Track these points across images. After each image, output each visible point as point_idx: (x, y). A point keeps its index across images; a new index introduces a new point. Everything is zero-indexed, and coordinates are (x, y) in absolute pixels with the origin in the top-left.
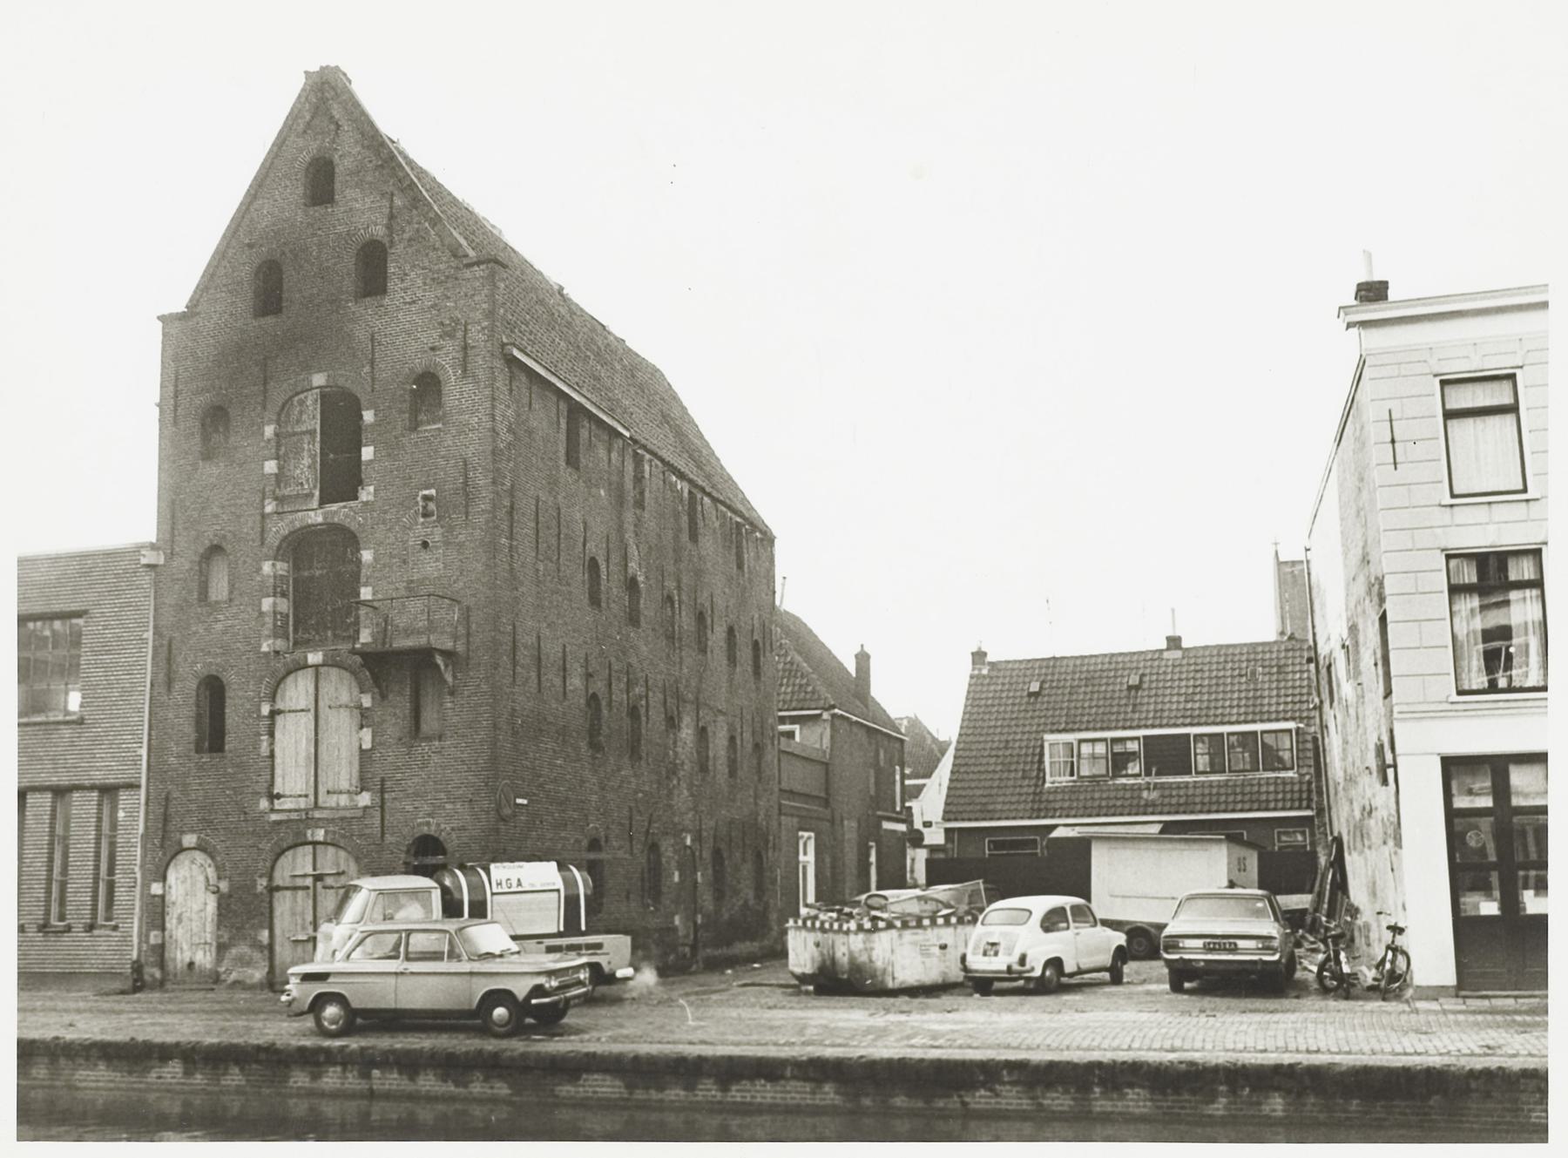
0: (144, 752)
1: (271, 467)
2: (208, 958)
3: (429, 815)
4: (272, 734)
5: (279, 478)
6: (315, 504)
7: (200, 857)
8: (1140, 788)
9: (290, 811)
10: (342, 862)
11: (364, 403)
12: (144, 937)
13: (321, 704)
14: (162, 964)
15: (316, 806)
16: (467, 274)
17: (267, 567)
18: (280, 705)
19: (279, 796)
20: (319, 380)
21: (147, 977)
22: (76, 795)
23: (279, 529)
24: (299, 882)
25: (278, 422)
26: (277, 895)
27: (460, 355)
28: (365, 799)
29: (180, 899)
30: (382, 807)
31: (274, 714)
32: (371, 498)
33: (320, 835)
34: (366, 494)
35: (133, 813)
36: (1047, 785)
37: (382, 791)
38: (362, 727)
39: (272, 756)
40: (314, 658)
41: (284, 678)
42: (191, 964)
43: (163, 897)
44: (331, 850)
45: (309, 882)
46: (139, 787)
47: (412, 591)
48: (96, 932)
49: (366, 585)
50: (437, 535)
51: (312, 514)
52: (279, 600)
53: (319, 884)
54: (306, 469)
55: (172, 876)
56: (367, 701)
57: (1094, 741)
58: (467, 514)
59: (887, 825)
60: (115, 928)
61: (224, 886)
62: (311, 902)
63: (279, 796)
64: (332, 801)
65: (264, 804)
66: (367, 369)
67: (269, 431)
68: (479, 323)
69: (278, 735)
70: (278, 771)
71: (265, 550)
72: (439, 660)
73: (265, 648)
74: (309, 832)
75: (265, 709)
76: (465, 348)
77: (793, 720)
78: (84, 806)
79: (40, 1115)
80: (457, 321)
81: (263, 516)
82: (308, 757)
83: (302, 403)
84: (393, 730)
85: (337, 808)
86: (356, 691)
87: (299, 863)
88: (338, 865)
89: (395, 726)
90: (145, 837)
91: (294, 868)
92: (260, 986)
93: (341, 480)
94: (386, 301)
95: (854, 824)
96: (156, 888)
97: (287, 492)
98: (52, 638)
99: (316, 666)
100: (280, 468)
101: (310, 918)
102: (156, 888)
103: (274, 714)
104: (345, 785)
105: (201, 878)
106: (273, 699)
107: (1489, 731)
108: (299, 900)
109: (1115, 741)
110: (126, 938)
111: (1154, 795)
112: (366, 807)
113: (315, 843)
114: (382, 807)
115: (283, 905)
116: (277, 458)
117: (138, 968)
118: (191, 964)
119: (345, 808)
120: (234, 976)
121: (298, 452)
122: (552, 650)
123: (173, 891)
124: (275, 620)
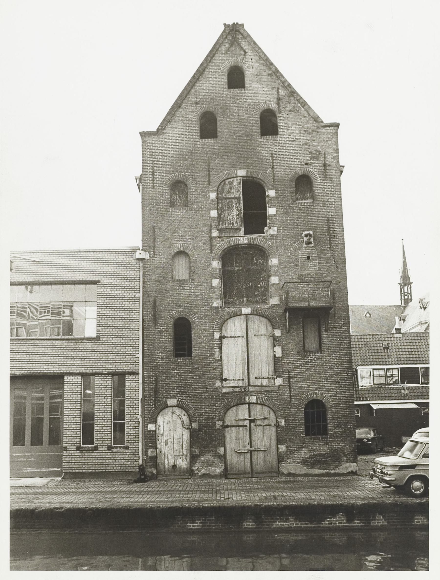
0: (140, 356)
2: (185, 462)
4: (220, 348)
7: (178, 411)
8: (399, 389)
9: (234, 387)
10: (266, 413)
12: (145, 453)
13: (249, 333)
14: (156, 466)
15: (249, 385)
16: (324, 130)
18: (224, 334)
19: (226, 380)
20: (242, 173)
21: (147, 472)
22: (97, 378)
23: (221, 245)
24: (240, 423)
26: (227, 430)
27: (323, 168)
28: (279, 381)
29: (166, 433)
30: (290, 386)
31: (222, 338)
32: (275, 233)
33: (253, 399)
35: (135, 388)
36: (360, 387)
37: (289, 378)
38: (274, 346)
39: (221, 359)
40: (246, 310)
42: (174, 466)
43: (155, 431)
44: (259, 407)
45: (247, 423)
46: (138, 374)
47: (302, 279)
49: (275, 275)
50: (314, 254)
51: (241, 238)
53: (252, 424)
54: (234, 215)
55: (160, 420)
56: (278, 333)
57: (379, 369)
58: (330, 245)
60: (127, 448)
61: (195, 425)
62: (248, 433)
63: (226, 380)
64: (258, 382)
65: (218, 384)
66: (269, 170)
67: (213, 196)
68: (332, 154)
69: (223, 348)
70: (225, 367)
71: (213, 255)
73: (215, 304)
74: (247, 398)
75: (217, 336)
76: (325, 165)
79: (21, 554)
80: (320, 153)
81: (211, 238)
82: (243, 359)
83: (231, 183)
84: (293, 348)
85: (262, 386)
86: (270, 329)
87: (242, 413)
88: (264, 414)
90: (143, 401)
91: (237, 416)
92: (220, 476)
94: (279, 138)
96: (151, 427)
97: (224, 226)
99: (246, 315)
101: (248, 440)
102: (151, 427)
103: (222, 338)
104: (265, 375)
105: (179, 422)
106: (221, 330)
108: (241, 433)
109: (388, 369)
110: (135, 453)
111: (407, 392)
112: (279, 386)
113: (249, 404)
114: (290, 386)
115: (231, 435)
116: (218, 209)
117: (142, 468)
118: (174, 466)
119: (267, 386)
120: (203, 471)
121: (230, 207)
123: (161, 428)
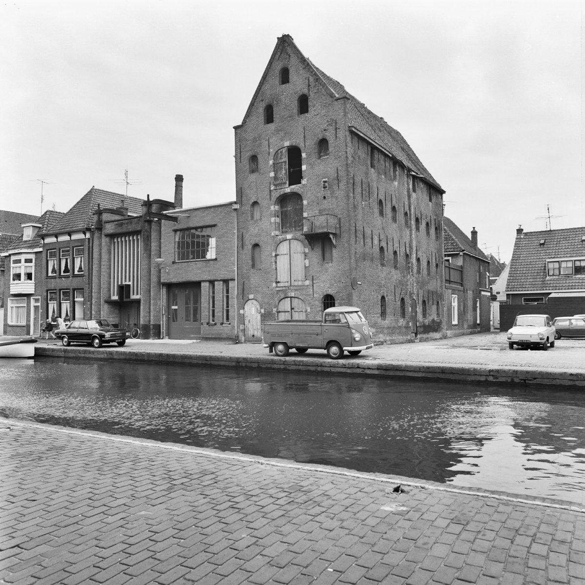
0: (236, 269)
5: (276, 178)
11: (302, 150)
17: (272, 208)
18: (278, 253)
23: (276, 195)
31: (276, 255)
52: (277, 218)
59: (483, 293)
65: (274, 285)
72: (331, 236)
75: (274, 254)
93: (295, 177)
95: (471, 292)
100: (275, 174)
102: (242, 312)
103: (276, 255)
107: (23, 261)
113: (291, 297)
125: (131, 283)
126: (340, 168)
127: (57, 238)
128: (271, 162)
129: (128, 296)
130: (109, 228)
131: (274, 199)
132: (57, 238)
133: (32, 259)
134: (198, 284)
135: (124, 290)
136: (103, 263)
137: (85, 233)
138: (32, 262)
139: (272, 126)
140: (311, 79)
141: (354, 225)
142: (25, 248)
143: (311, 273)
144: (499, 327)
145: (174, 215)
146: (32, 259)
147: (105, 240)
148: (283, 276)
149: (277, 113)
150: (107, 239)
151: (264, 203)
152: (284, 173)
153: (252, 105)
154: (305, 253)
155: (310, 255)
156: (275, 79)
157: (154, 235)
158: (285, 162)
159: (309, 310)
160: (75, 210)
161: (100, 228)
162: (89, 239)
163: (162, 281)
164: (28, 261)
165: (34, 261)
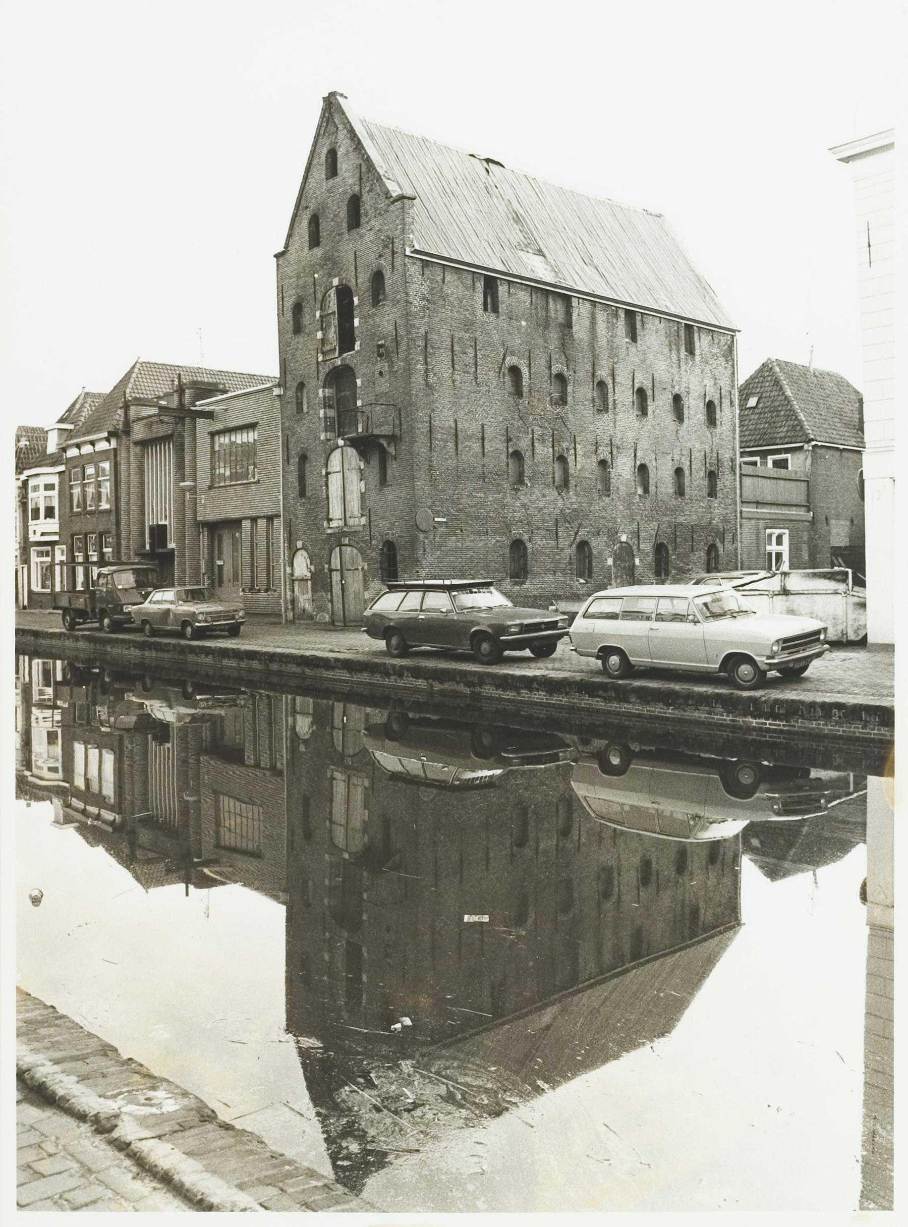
0: (281, 497)
1: (319, 335)
3: (389, 529)
5: (323, 341)
6: (337, 354)
11: (354, 293)
19: (331, 520)
23: (324, 370)
25: (321, 309)
34: (357, 346)
38: (361, 480)
41: (330, 454)
48: (269, 593)
52: (328, 410)
63: (331, 520)
65: (325, 524)
77: (787, 451)
78: (262, 524)
81: (318, 363)
89: (374, 476)
93: (347, 340)
98: (29, 455)
100: (324, 335)
103: (328, 474)
107: (42, 487)
121: (329, 326)
122: (470, 427)
124: (326, 422)
125: (167, 523)
126: (399, 321)
127: (79, 449)
128: (318, 314)
129: (164, 545)
130: (139, 432)
131: (322, 376)
132: (79, 449)
133: (54, 485)
134: (236, 523)
135: (159, 532)
136: (132, 490)
137: (108, 440)
138: (54, 489)
139: (318, 252)
140: (364, 169)
141: (427, 419)
142: (47, 465)
143: (370, 503)
144: (58, 530)
145: (207, 409)
146: (54, 485)
147: (135, 450)
148: (336, 511)
149: (325, 226)
150: (138, 449)
151: (311, 384)
152: (333, 334)
153: (295, 216)
154: (360, 468)
155: (366, 474)
156: (320, 173)
157: (187, 441)
158: (334, 313)
159: (366, 567)
160: (401, 140)
161: (127, 432)
162: (115, 450)
163: (199, 519)
164: (49, 487)
165: (57, 487)
